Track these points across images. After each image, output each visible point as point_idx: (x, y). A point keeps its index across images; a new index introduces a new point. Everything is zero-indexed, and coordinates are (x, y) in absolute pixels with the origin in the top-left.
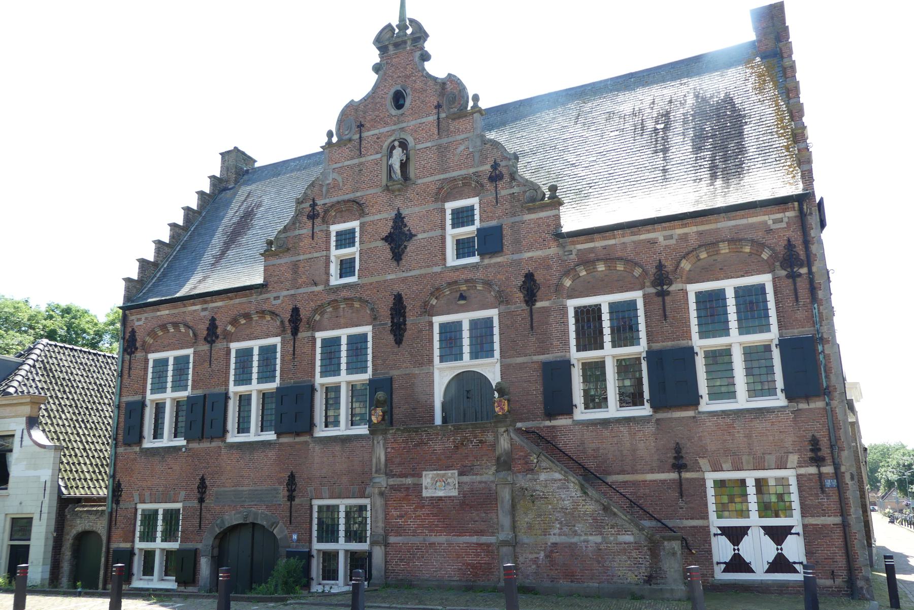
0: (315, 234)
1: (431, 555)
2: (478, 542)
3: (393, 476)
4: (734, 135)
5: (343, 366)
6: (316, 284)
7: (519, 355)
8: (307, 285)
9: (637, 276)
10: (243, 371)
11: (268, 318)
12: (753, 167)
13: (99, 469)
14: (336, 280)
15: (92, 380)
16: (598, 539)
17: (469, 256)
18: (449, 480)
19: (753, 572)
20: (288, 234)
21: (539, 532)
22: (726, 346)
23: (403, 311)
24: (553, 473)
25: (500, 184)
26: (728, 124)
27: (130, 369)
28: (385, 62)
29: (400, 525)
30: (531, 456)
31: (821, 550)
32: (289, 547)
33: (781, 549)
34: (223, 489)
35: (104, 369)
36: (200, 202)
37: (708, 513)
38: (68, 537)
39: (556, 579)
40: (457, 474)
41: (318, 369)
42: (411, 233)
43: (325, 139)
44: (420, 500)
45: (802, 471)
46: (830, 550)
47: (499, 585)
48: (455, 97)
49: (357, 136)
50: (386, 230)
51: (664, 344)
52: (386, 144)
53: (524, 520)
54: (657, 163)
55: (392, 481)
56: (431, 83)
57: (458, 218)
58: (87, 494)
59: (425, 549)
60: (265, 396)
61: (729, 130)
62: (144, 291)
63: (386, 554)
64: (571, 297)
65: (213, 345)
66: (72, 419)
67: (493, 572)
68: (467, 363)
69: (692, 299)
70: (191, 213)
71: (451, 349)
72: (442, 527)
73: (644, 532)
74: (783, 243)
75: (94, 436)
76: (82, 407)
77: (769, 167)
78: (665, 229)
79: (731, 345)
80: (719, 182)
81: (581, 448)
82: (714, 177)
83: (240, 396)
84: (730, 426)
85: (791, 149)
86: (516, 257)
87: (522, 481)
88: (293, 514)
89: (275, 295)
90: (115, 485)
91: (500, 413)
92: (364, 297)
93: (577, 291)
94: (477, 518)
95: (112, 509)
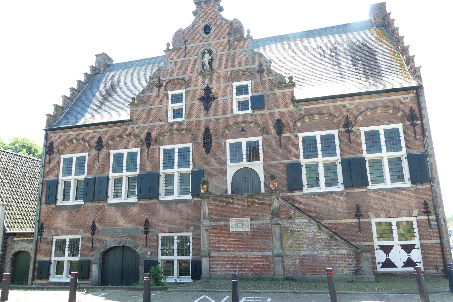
0: (160, 95)
1: (235, 262)
2: (262, 255)
3: (213, 221)
4: (372, 60)
5: (176, 164)
6: (161, 121)
7: (274, 160)
8: (156, 121)
9: (335, 122)
10: (118, 166)
11: (133, 138)
12: (386, 74)
13: (26, 217)
14: (171, 119)
15: (19, 169)
16: (328, 252)
17: (245, 110)
18: (245, 223)
19: (396, 267)
20: (145, 94)
21: (296, 249)
22: (379, 158)
23: (210, 136)
24: (303, 219)
25: (263, 75)
26: (368, 55)
27: (49, 163)
28: (199, 10)
29: (217, 246)
30: (290, 210)
31: (430, 256)
32: (145, 258)
33: (410, 256)
34: (106, 228)
35: (25, 164)
36: (85, 79)
37: (373, 239)
38: (9, 254)
39: (306, 273)
40: (249, 220)
41: (161, 165)
42: (214, 97)
43: (166, 47)
44: (229, 233)
45: (420, 218)
46: (434, 256)
47: (274, 277)
48: (238, 30)
49: (184, 46)
50: (201, 94)
51: (350, 156)
52: (200, 52)
53: (287, 243)
54: (336, 70)
55: (212, 223)
56: (224, 22)
57: (240, 90)
58: (20, 231)
59: (232, 259)
60: (78, 182)
61: (369, 57)
62: (57, 122)
63: (210, 262)
64: (300, 132)
65: (100, 151)
66: (9, 190)
67: (270, 270)
68: (245, 163)
69: (363, 134)
70: (81, 83)
71: (236, 156)
72: (241, 247)
73: (352, 249)
74: (408, 109)
75: (22, 199)
76: (14, 184)
77: (394, 74)
78: (350, 100)
79: (318, 162)
80: (371, 80)
81: (307, 207)
82: (367, 77)
83: (65, 182)
84: (384, 196)
85: (403, 67)
86: (271, 111)
87: (286, 223)
88: (147, 241)
89: (137, 126)
90: (40, 226)
91: (273, 188)
92: (188, 128)
93: (303, 129)
94: (261, 243)
95: (38, 239)
